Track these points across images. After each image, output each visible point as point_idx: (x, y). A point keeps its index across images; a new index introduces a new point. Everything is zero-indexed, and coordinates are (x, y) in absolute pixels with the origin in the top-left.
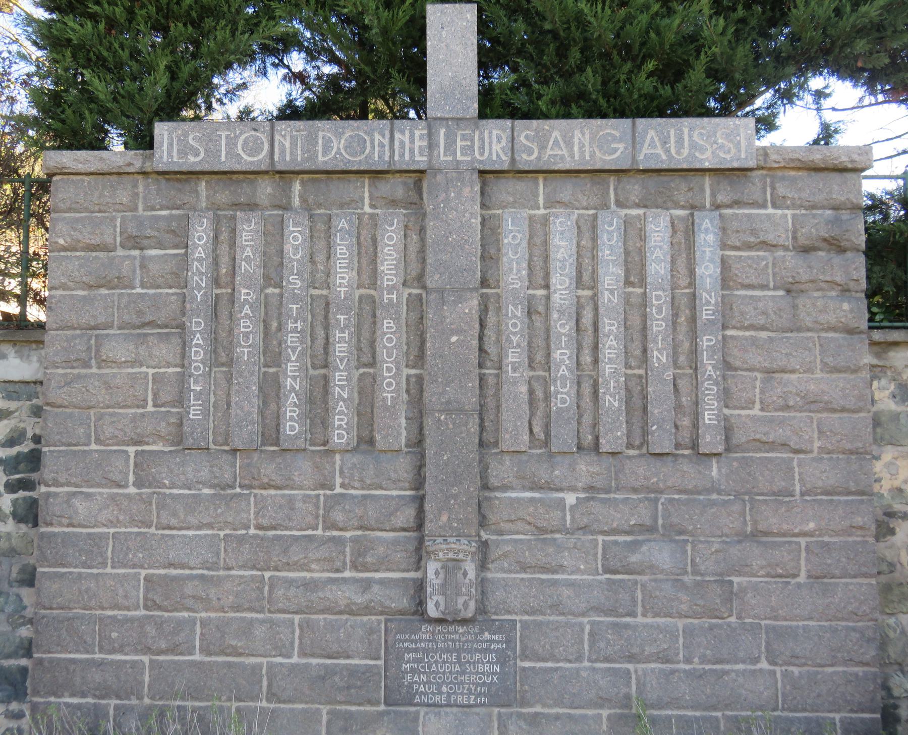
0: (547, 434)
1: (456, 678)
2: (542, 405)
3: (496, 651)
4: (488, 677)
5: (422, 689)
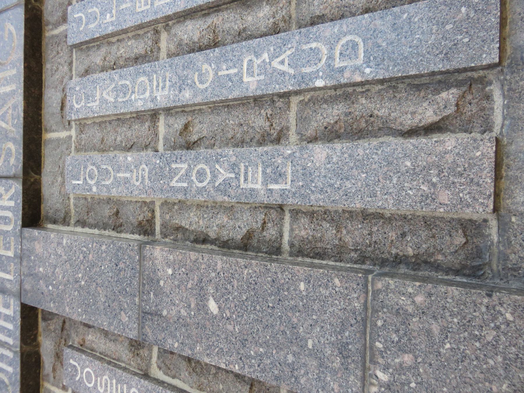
0: (441, 80)
2: (363, 105)
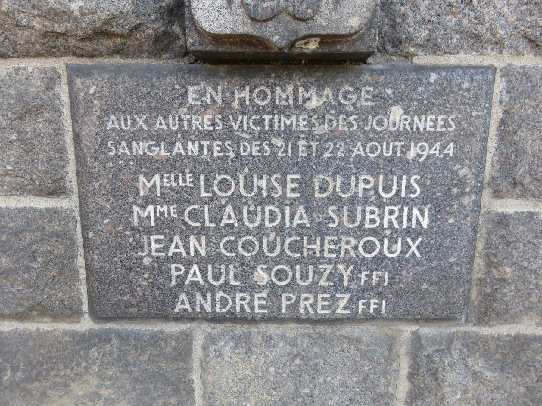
1: (296, 247)
3: (423, 167)
4: (393, 241)
5: (195, 275)
